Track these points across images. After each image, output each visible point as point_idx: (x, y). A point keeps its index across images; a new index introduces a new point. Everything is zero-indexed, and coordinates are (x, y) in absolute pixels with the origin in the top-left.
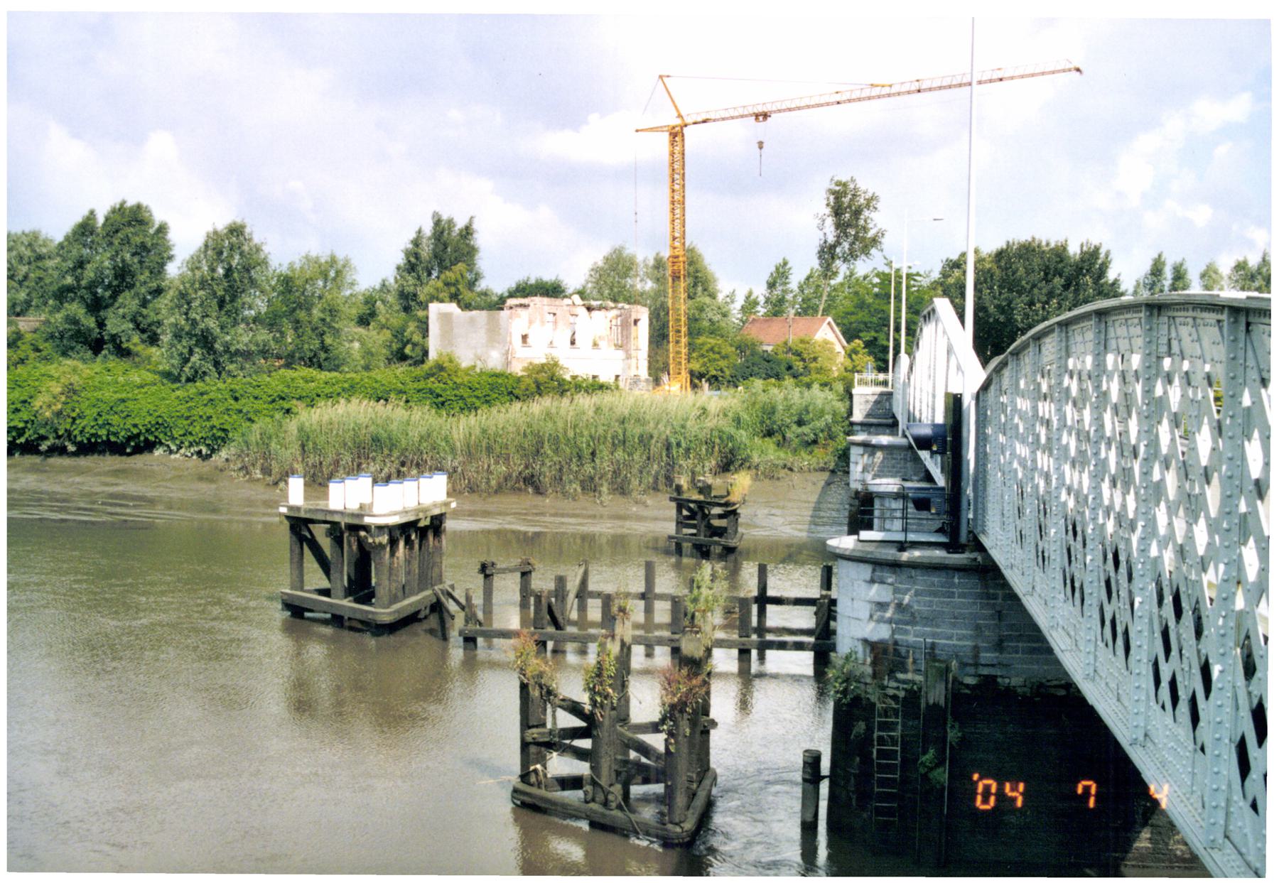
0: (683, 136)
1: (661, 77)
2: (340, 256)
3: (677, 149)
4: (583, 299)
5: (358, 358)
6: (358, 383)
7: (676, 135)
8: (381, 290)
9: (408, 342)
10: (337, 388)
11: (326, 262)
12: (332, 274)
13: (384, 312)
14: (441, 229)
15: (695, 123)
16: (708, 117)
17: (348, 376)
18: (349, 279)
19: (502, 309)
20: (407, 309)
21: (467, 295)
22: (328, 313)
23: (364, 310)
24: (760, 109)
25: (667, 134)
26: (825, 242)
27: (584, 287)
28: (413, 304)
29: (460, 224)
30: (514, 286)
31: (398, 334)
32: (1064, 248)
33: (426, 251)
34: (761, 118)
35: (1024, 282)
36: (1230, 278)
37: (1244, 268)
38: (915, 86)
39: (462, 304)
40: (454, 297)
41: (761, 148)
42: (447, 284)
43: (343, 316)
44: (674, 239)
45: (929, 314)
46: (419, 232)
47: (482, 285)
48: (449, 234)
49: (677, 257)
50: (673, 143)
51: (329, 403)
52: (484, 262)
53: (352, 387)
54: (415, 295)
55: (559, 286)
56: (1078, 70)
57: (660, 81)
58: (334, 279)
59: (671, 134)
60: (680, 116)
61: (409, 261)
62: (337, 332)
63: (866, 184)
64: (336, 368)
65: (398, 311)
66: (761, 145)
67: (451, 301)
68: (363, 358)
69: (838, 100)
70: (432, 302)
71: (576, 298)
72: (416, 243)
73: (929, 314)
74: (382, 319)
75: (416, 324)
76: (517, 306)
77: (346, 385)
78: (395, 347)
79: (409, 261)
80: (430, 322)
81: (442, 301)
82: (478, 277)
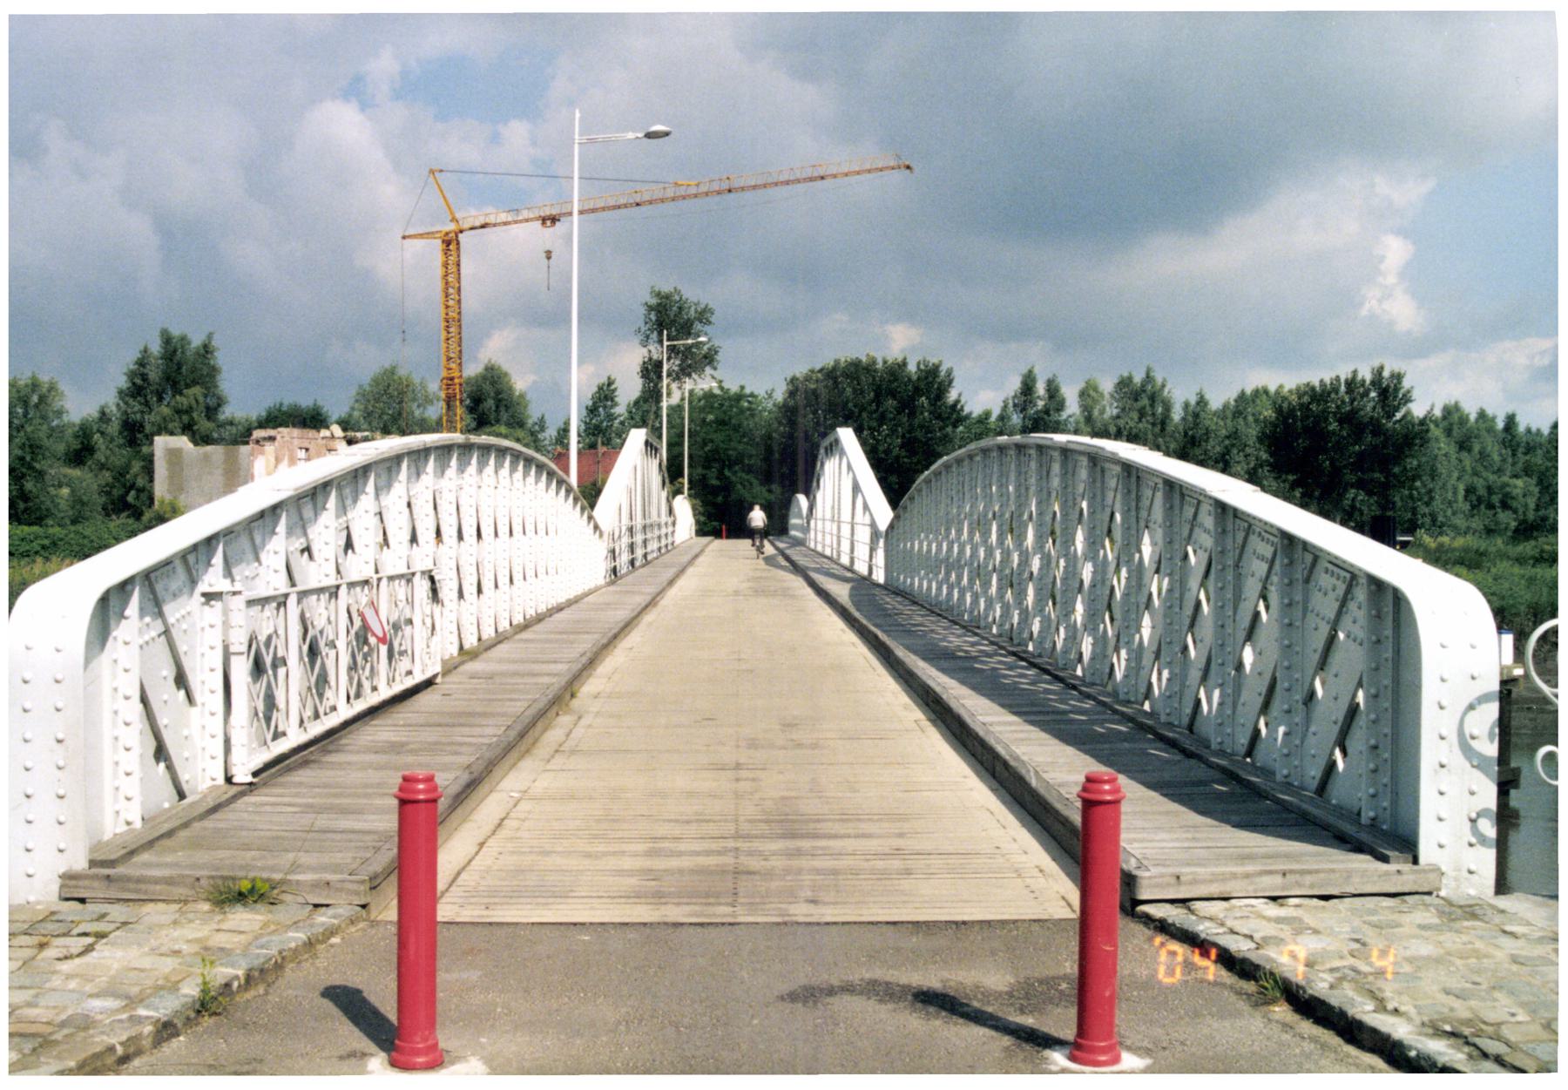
0: (458, 243)
1: (432, 172)
2: (44, 378)
3: (452, 259)
4: (345, 430)
5: (66, 508)
6: (61, 540)
7: (450, 243)
8: (101, 419)
9: (132, 486)
10: (36, 546)
11: (27, 386)
12: (35, 399)
13: (103, 447)
14: (172, 348)
15: (472, 229)
16: (488, 221)
17: (51, 531)
18: (57, 405)
19: (247, 443)
20: (132, 442)
21: (204, 425)
22: (27, 449)
23: (76, 445)
24: (547, 212)
25: (439, 242)
26: (650, 359)
27: (350, 415)
28: (139, 436)
29: (196, 341)
30: (264, 414)
31: (121, 474)
32: (904, 364)
33: (154, 375)
34: (548, 223)
35: (850, 405)
36: (1112, 396)
37: (1128, 386)
38: (725, 186)
39: (197, 437)
40: (188, 429)
41: (549, 258)
42: (178, 412)
43: (47, 454)
44: (449, 359)
45: (831, 445)
46: (145, 350)
47: (227, 413)
48: (183, 353)
49: (452, 379)
50: (446, 252)
51: (22, 563)
52: (228, 384)
53: (54, 544)
54: (142, 426)
55: (319, 414)
56: (908, 167)
57: (431, 179)
58: (37, 406)
59: (443, 241)
60: (454, 220)
61: (134, 384)
62: (40, 475)
63: (694, 294)
64: (39, 521)
65: (119, 447)
66: (549, 255)
67: (183, 434)
68: (73, 508)
69: (638, 200)
70: (159, 434)
71: (337, 430)
72: (142, 363)
73: (831, 445)
74: (100, 456)
75: (142, 463)
76: (265, 439)
77: (46, 542)
78: (116, 492)
79: (134, 384)
80: (156, 458)
81: (172, 434)
82: (221, 402)
